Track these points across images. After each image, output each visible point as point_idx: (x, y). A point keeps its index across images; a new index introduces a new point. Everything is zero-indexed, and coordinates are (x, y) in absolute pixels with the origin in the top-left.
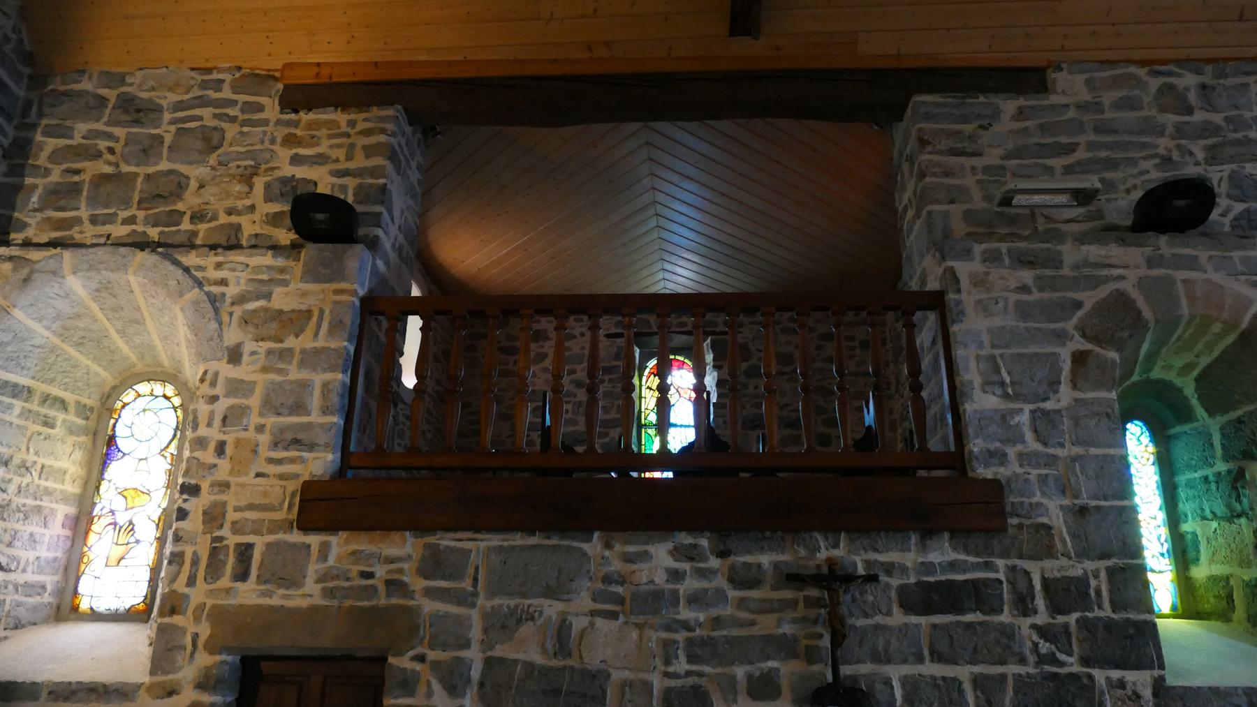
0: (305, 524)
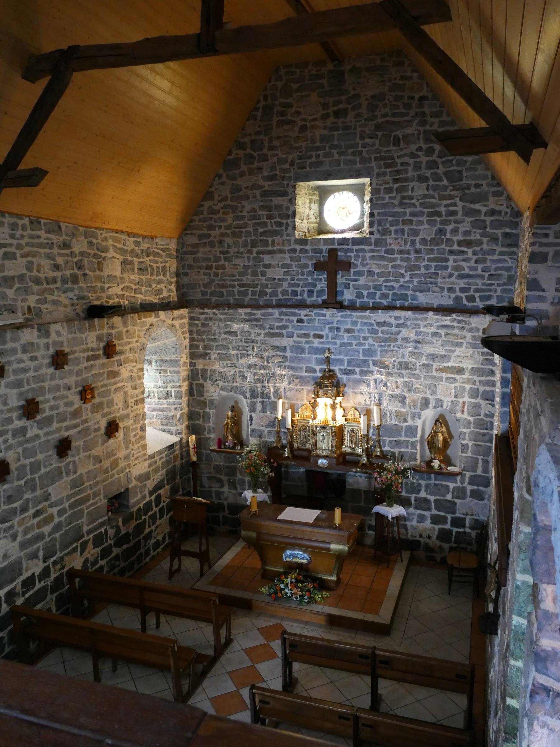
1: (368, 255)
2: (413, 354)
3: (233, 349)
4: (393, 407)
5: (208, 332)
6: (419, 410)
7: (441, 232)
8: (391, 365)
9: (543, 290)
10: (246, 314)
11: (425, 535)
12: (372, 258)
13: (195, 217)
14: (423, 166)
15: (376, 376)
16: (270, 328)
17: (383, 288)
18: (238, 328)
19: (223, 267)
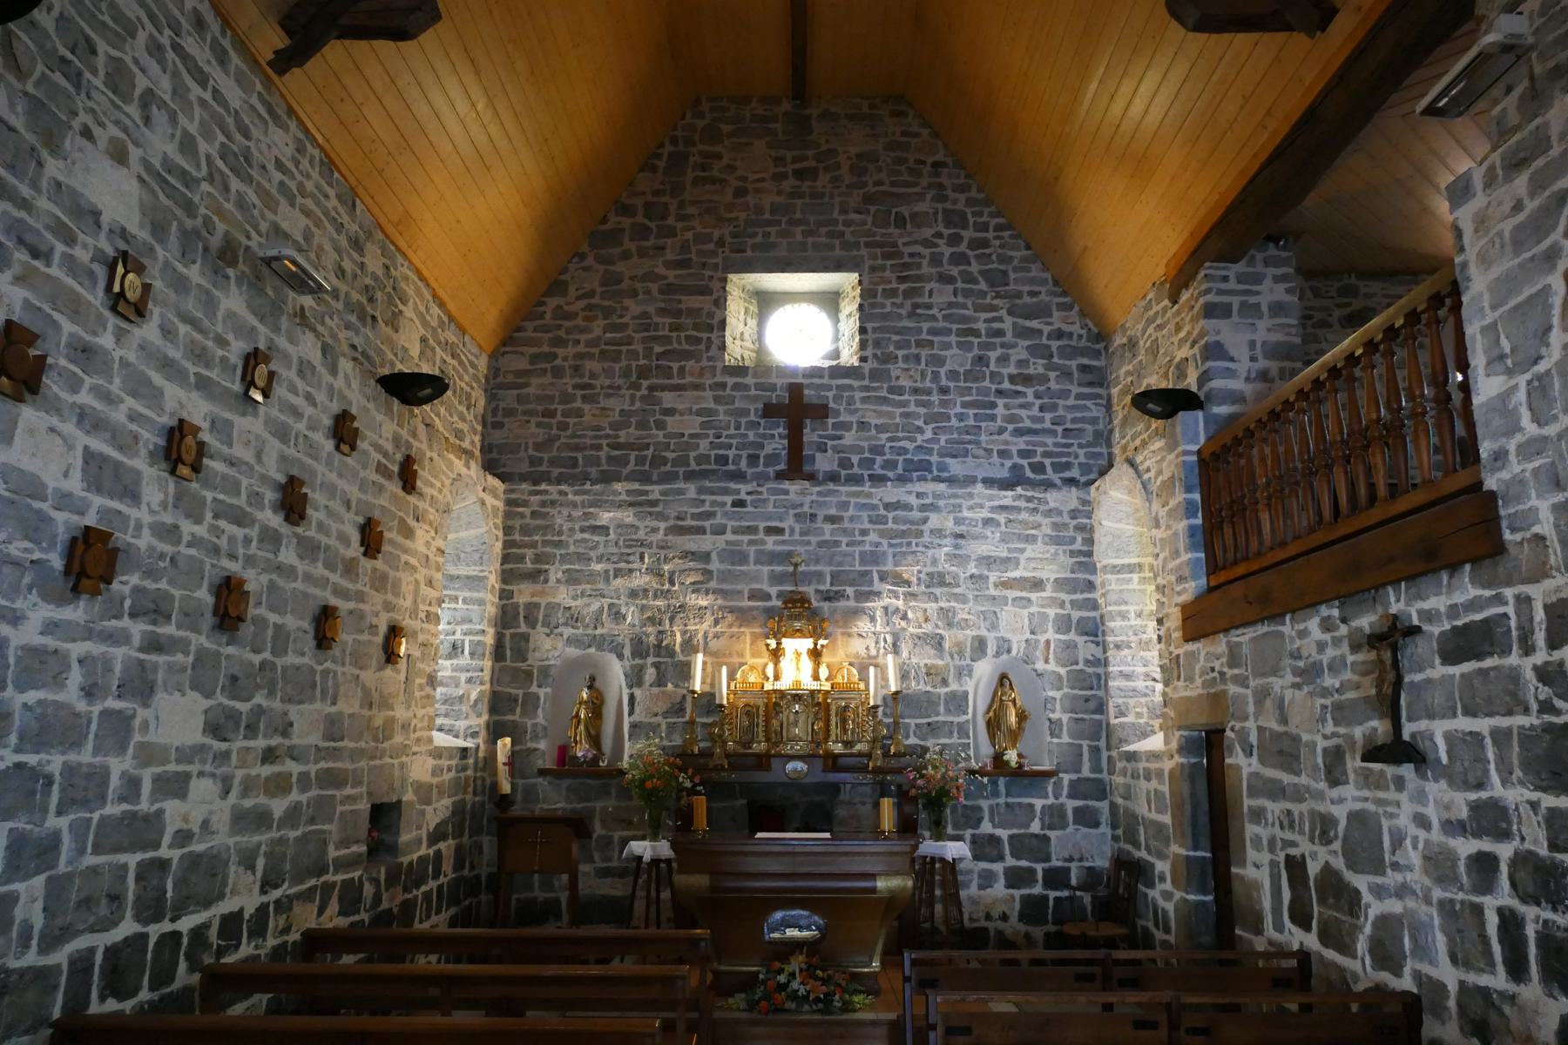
0: (1189, 637)
1: (858, 395)
2: (952, 557)
3: (600, 559)
4: (924, 658)
5: (545, 529)
6: (968, 661)
7: (981, 360)
8: (914, 580)
9: (1232, 359)
10: (629, 492)
11: (995, 914)
12: (864, 400)
13: (526, 324)
14: (945, 261)
15: (887, 601)
16: (678, 518)
17: (887, 450)
18: (611, 519)
19: (579, 413)
